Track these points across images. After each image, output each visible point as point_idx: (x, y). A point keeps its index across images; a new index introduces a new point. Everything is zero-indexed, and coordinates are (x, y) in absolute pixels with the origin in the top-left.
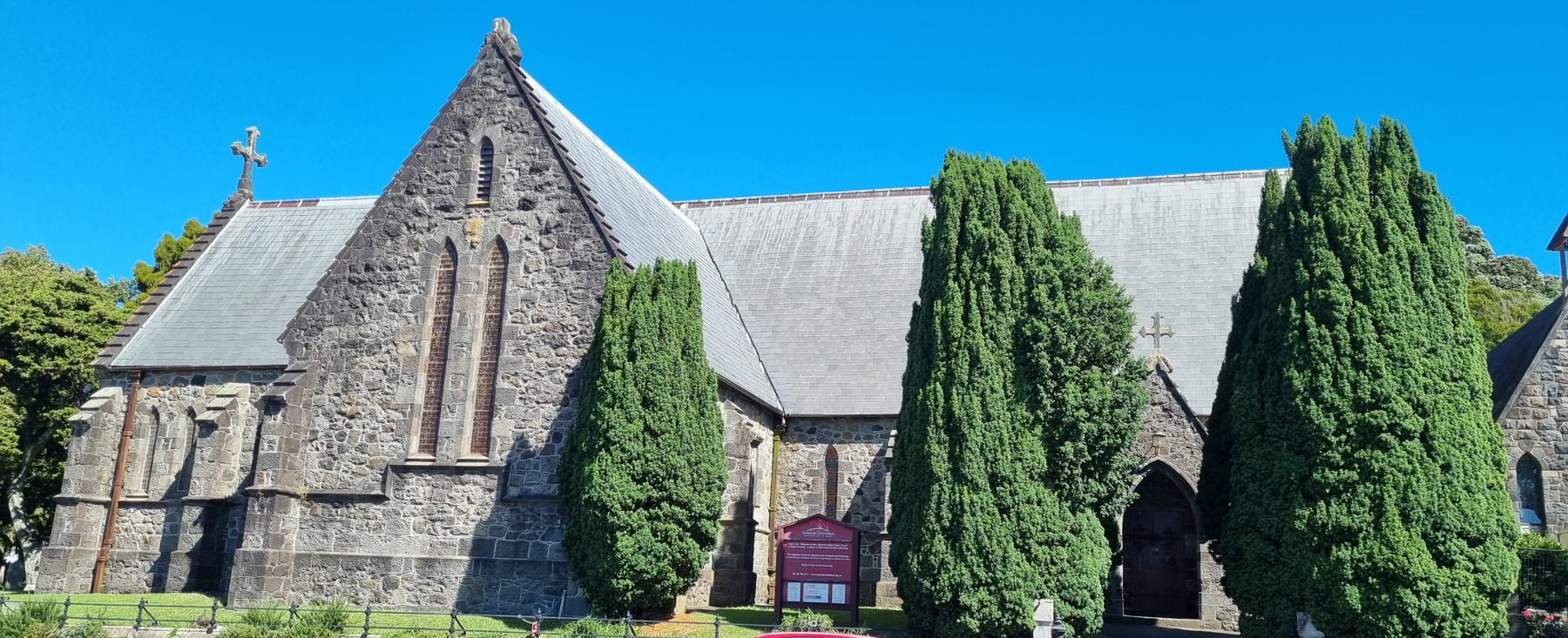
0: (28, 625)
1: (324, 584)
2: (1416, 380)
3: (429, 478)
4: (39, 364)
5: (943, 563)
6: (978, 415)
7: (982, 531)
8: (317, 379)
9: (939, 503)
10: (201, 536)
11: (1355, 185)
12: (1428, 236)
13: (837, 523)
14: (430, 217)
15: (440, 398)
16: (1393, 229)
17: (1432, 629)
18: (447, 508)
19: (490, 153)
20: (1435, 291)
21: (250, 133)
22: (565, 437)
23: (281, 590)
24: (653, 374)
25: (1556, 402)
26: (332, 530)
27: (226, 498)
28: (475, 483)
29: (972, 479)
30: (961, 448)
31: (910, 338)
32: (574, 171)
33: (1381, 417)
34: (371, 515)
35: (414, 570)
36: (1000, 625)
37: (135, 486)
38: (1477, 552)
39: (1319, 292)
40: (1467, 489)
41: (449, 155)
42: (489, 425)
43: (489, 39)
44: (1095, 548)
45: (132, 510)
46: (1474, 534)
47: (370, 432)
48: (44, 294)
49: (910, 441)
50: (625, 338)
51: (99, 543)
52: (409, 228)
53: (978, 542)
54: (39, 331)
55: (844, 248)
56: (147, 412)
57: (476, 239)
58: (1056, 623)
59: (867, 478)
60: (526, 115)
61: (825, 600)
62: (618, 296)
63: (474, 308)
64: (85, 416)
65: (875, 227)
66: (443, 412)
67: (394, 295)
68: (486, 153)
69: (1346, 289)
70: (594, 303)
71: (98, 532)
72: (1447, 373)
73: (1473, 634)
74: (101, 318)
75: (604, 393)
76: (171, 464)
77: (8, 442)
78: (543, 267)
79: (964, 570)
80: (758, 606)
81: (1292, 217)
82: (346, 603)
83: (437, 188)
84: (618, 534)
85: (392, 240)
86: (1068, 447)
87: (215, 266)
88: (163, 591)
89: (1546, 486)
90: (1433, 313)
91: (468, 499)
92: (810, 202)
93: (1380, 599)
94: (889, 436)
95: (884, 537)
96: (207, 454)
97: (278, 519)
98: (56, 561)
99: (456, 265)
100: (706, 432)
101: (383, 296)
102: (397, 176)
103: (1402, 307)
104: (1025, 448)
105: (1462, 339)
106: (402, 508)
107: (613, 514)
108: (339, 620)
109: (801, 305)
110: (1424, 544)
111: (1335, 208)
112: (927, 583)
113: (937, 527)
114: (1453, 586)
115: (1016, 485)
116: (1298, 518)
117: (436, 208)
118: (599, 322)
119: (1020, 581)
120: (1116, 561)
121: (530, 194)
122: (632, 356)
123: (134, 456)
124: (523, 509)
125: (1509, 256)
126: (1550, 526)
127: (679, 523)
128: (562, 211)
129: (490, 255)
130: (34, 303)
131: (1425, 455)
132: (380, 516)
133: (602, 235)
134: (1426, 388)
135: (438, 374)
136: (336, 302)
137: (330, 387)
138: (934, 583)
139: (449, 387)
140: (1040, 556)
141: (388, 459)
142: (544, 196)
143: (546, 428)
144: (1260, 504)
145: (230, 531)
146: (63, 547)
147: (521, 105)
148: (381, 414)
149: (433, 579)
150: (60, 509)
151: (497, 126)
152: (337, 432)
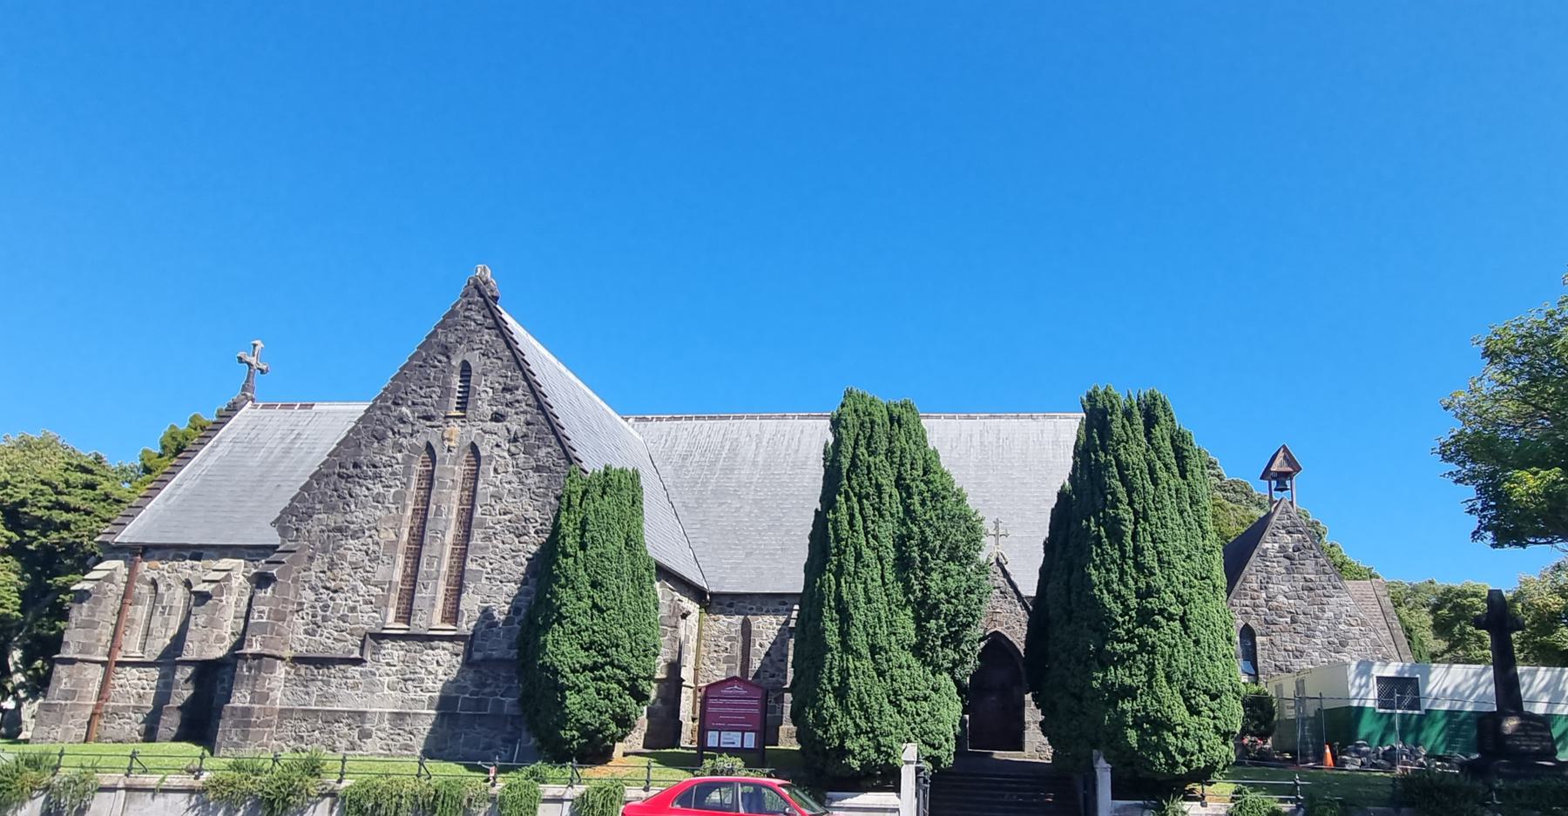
0: (21, 774)
1: (305, 734)
2: (1177, 577)
3: (403, 644)
4: (45, 537)
5: (833, 716)
6: (862, 599)
7: (863, 691)
8: (306, 559)
9: (831, 669)
10: (191, 692)
11: (1135, 435)
12: (1188, 474)
13: (749, 683)
14: (413, 425)
15: (416, 577)
16: (1160, 468)
17: (1185, 761)
18: (418, 670)
19: (469, 374)
20: (1191, 514)
21: (255, 345)
22: (524, 611)
23: (265, 740)
24: (602, 561)
25: (1266, 587)
26: (313, 688)
27: (217, 659)
28: (444, 649)
29: (857, 649)
30: (848, 625)
31: (812, 537)
32: (540, 392)
33: (1153, 603)
34: (349, 675)
35: (386, 722)
36: (876, 765)
37: (132, 647)
38: (1215, 705)
39: (1111, 511)
40: (1210, 657)
41: (432, 374)
42: (458, 600)
43: (471, 281)
44: (950, 702)
45: (128, 668)
46: (1214, 691)
47: (351, 604)
48: (52, 472)
49: (810, 619)
50: (577, 531)
51: (94, 696)
52: (394, 433)
53: (860, 699)
54: (45, 507)
55: (760, 459)
56: (146, 583)
57: (453, 444)
58: (918, 762)
59: (774, 643)
60: (501, 344)
61: (738, 745)
62: (573, 497)
63: (449, 502)
64: (87, 586)
65: (785, 443)
66: (417, 588)
67: (378, 488)
68: (465, 374)
69: (1130, 510)
70: (553, 500)
71: (95, 688)
72: (1198, 574)
73: (1212, 764)
74: (107, 497)
75: (557, 576)
76: (167, 629)
77: (10, 605)
78: (510, 469)
79: (849, 722)
80: (683, 748)
81: (1093, 456)
82: (325, 751)
83: (420, 400)
84: (567, 693)
85: (378, 443)
86: (932, 624)
87: (216, 458)
88: (154, 741)
89: (1259, 647)
90: (1189, 529)
91: (438, 662)
92: (735, 421)
93: (1151, 739)
94: (792, 610)
95: (787, 690)
96: (201, 620)
97: (265, 679)
98: (52, 714)
99: (434, 466)
100: (644, 608)
101: (368, 489)
102: (386, 389)
103: (1170, 524)
104: (898, 624)
105: (1208, 549)
106: (378, 669)
107: (563, 676)
108: (318, 767)
109: (723, 503)
110: (1182, 699)
111: (1122, 451)
112: (820, 732)
113: (829, 688)
114: (1199, 729)
115: (890, 653)
116: (1095, 679)
117: (419, 417)
118: (557, 518)
119: (893, 729)
120: (964, 712)
121: (501, 409)
122: (583, 547)
123: (133, 621)
124: (485, 671)
125: (1235, 479)
126: (1261, 676)
127: (619, 682)
128: (528, 424)
129: (464, 458)
130: (43, 482)
131: (1183, 633)
132: (358, 676)
133: (562, 446)
134: (1184, 583)
135: (415, 556)
136: (326, 493)
137: (316, 565)
138: (825, 733)
139: (423, 567)
140: (908, 709)
141: (366, 627)
142: (513, 411)
143: (508, 603)
144: (1068, 669)
145: (219, 688)
146: (60, 702)
147: (497, 336)
148: (362, 589)
149: (404, 730)
150: (58, 668)
151: (477, 352)
152: (321, 604)
